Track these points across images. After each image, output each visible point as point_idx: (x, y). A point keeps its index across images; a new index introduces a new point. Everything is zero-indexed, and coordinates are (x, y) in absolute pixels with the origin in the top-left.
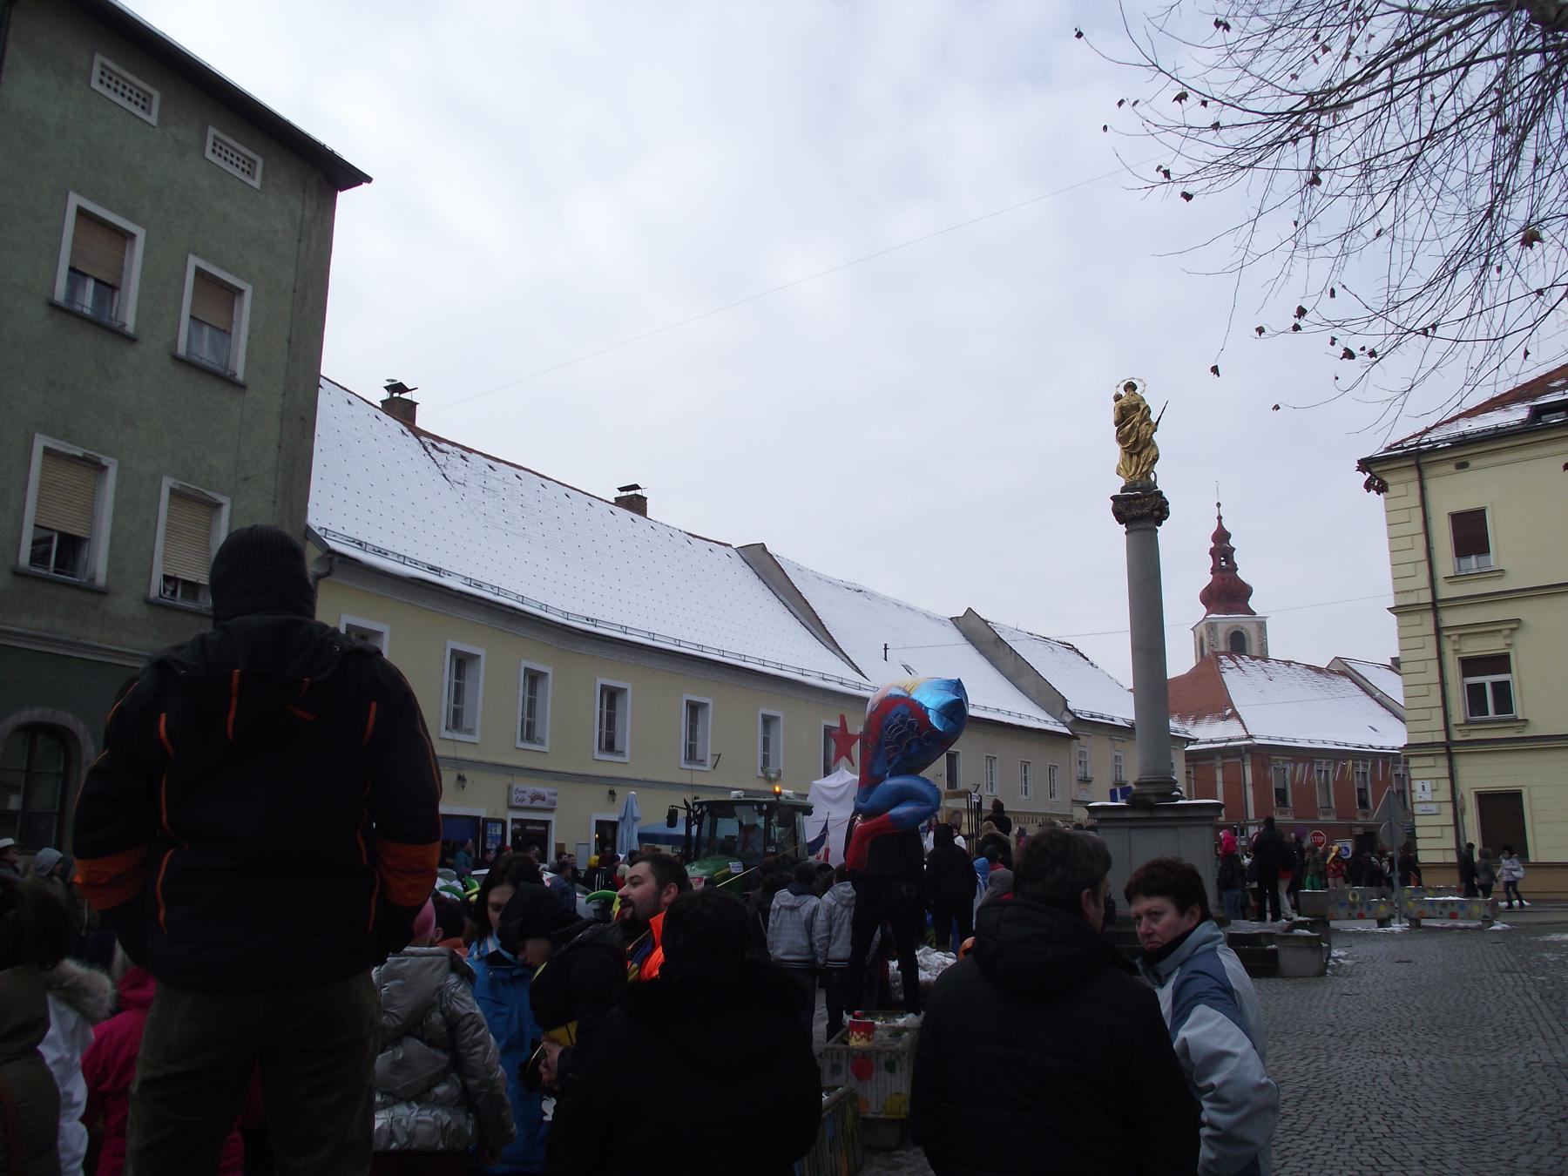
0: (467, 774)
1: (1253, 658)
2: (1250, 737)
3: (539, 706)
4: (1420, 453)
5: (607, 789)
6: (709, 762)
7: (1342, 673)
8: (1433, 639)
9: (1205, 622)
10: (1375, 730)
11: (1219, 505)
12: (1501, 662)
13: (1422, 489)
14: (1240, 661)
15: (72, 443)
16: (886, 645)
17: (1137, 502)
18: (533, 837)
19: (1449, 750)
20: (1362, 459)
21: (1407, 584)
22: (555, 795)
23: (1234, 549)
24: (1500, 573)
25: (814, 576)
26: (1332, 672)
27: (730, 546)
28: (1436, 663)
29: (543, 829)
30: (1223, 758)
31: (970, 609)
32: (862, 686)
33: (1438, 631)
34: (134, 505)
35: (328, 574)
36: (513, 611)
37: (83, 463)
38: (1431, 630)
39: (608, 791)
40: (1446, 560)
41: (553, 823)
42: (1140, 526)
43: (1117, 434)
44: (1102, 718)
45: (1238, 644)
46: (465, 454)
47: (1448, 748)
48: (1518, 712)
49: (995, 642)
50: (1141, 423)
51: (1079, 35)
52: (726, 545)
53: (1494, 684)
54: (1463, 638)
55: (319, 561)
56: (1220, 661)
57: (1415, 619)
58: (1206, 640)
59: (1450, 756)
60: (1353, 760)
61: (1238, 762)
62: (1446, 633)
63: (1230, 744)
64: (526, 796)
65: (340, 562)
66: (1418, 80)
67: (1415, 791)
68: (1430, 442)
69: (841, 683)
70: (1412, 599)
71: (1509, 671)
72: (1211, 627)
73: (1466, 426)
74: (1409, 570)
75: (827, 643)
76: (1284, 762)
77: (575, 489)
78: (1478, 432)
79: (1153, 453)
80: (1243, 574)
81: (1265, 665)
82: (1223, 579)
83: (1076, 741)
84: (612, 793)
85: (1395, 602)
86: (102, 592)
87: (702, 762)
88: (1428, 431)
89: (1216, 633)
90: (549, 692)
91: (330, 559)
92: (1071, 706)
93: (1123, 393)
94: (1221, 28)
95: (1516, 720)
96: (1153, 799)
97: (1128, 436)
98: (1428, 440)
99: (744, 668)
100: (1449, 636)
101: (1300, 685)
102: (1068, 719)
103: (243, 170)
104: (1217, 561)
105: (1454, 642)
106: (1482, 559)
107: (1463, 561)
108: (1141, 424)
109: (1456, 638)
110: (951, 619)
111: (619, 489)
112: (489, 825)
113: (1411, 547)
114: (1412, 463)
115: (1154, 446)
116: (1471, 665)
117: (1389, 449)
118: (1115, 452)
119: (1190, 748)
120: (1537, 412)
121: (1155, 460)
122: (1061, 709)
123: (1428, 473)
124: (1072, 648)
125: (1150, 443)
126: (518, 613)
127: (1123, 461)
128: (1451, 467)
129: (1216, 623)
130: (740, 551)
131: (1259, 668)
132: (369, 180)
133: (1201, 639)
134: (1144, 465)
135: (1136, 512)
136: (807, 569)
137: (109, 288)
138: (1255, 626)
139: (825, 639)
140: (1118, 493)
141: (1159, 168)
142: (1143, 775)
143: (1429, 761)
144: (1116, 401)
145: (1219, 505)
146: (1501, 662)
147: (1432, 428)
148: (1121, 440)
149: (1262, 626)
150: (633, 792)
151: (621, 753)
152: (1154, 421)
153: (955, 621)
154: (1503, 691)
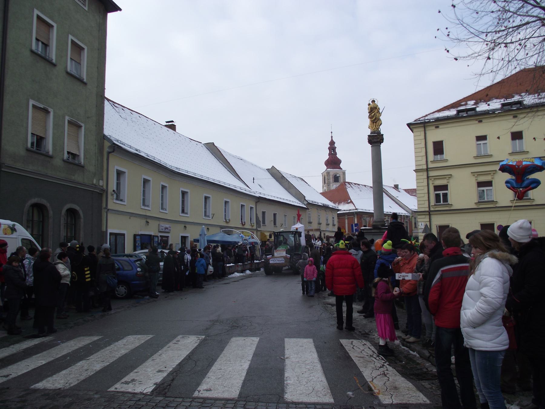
0: (149, 221)
2: (356, 209)
3: (164, 197)
4: (425, 123)
5: (184, 225)
6: (211, 216)
8: (426, 180)
9: (326, 171)
10: (391, 207)
11: (332, 132)
12: (445, 187)
15: (40, 103)
16: (254, 178)
17: (376, 137)
18: (164, 242)
19: (429, 213)
20: (408, 124)
21: (419, 163)
22: (170, 227)
23: (336, 148)
24: (446, 161)
27: (201, 143)
29: (167, 239)
30: (348, 216)
31: (273, 166)
33: (428, 177)
34: (58, 126)
35: (113, 152)
36: (160, 165)
37: (42, 110)
38: (426, 177)
39: (184, 226)
41: (170, 237)
42: (376, 145)
44: (315, 202)
46: (123, 108)
47: (429, 213)
48: (450, 202)
49: (282, 178)
51: (439, 12)
53: (443, 193)
54: (435, 180)
55: (110, 147)
56: (346, 185)
57: (421, 174)
58: (326, 177)
59: (430, 215)
60: (388, 217)
61: (353, 217)
62: (430, 178)
63: (350, 211)
64: (163, 228)
65: (117, 147)
67: (419, 225)
68: (428, 119)
70: (420, 168)
72: (328, 173)
74: (420, 158)
75: (236, 177)
76: (367, 217)
77: (156, 122)
78: (442, 117)
79: (381, 123)
80: (339, 156)
81: (359, 186)
82: (332, 157)
83: (308, 210)
84: (185, 227)
86: (51, 157)
87: (208, 216)
88: (426, 116)
89: (330, 175)
90: (168, 191)
91: (114, 147)
92: (306, 199)
95: (449, 204)
96: (380, 226)
97: (373, 117)
99: (219, 185)
100: (431, 179)
101: (369, 193)
102: (306, 203)
103: (82, 3)
104: (331, 151)
105: (432, 181)
106: (441, 156)
107: (436, 156)
108: (377, 113)
109: (433, 180)
110: (267, 169)
111: (166, 122)
112: (155, 237)
114: (423, 125)
115: (381, 120)
116: (437, 188)
117: (416, 121)
118: (368, 122)
119: (338, 212)
120: (459, 112)
121: (381, 125)
122: (303, 200)
123: (427, 129)
124: (303, 180)
125: (379, 120)
126: (162, 166)
128: (434, 128)
129: (330, 172)
132: (120, 10)
133: (325, 177)
134: (378, 126)
135: (375, 140)
137: (46, 46)
138: (342, 173)
139: (236, 175)
140: (370, 134)
141: (446, 50)
142: (377, 219)
143: (423, 216)
145: (332, 132)
146: (445, 187)
147: (428, 115)
148: (370, 117)
149: (344, 173)
150: (204, 226)
151: (187, 213)
152: (381, 112)
154: (445, 195)
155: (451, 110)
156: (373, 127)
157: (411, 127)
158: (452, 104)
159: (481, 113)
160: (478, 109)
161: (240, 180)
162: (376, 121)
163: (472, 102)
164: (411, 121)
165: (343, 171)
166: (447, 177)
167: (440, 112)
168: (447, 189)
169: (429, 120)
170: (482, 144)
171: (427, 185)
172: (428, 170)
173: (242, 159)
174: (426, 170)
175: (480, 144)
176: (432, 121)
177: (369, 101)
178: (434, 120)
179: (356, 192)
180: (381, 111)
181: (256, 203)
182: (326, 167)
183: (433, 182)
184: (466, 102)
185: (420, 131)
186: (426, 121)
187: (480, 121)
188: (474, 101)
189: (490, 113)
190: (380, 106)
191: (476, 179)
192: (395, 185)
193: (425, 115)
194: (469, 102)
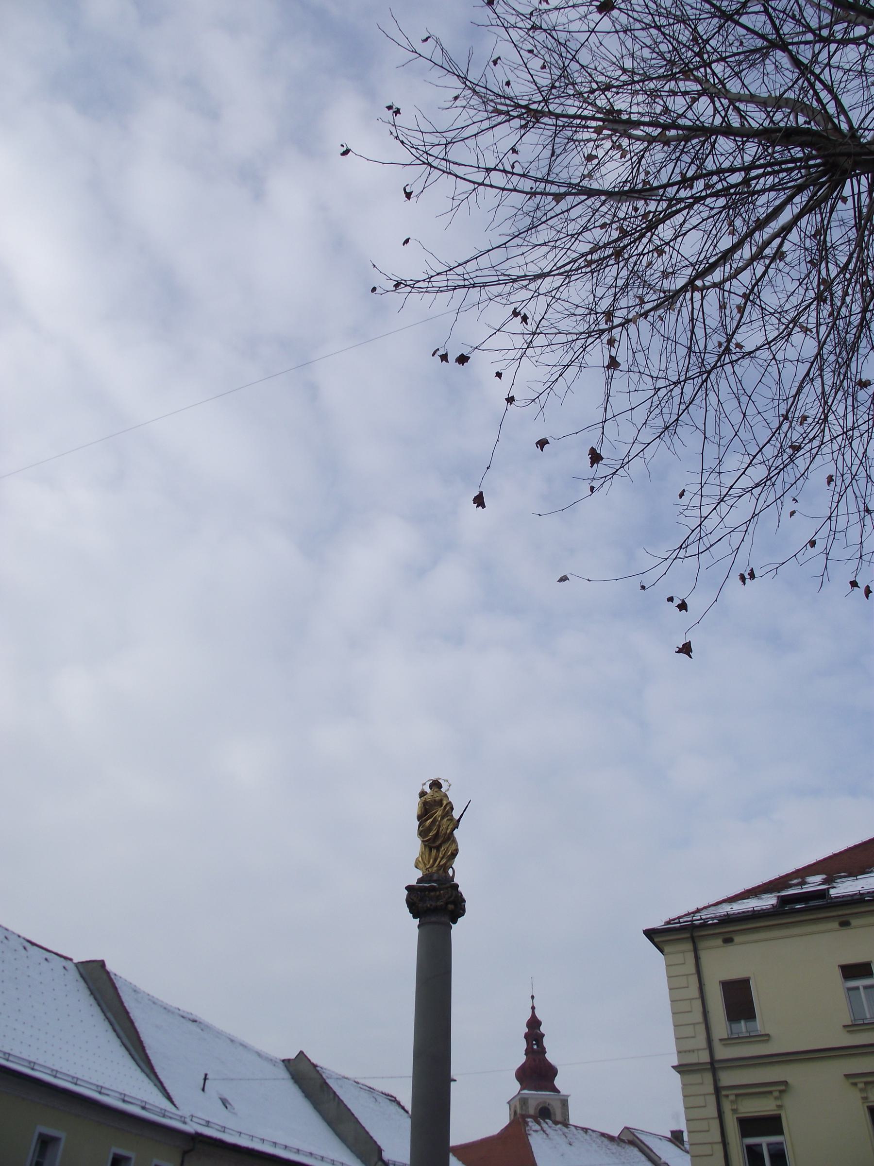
1: (556, 1123)
7: (632, 1143)
9: (519, 1097)
11: (533, 997)
13: (697, 959)
14: (544, 1125)
16: (206, 1075)
17: (432, 894)
24: (766, 1038)
25: (149, 1000)
26: (623, 1141)
27: (71, 960)
28: (717, 1122)
31: (301, 1053)
32: (166, 1114)
38: (711, 1089)
40: (720, 1026)
42: (433, 919)
43: (419, 827)
45: (544, 1113)
50: (443, 818)
52: (66, 958)
53: (768, 1145)
56: (527, 1123)
57: (695, 1078)
62: (724, 1093)
66: (743, 173)
68: (701, 919)
69: (144, 1108)
70: (692, 1059)
71: (780, 1132)
72: (524, 1101)
73: (726, 909)
79: (453, 847)
81: (565, 1130)
85: (678, 1060)
88: (698, 911)
89: (528, 1108)
93: (428, 790)
94: (519, 318)
97: (429, 829)
98: (699, 918)
100: (727, 1096)
106: (750, 1024)
107: (735, 1026)
110: (283, 1061)
113: (689, 1009)
114: (688, 935)
117: (668, 923)
118: (415, 846)
121: (454, 854)
123: (701, 945)
125: (450, 838)
127: (422, 854)
128: (719, 942)
130: (80, 967)
131: (561, 1133)
134: (442, 858)
136: (144, 992)
140: (414, 882)
144: (420, 798)
145: (533, 997)
147: (702, 909)
148: (422, 833)
149: (564, 1103)
153: (287, 1062)
155: (764, 896)
156: (429, 862)
157: (656, 940)
158: (765, 884)
159: (843, 901)
160: (833, 892)
161: (153, 1077)
162: (438, 843)
163: (819, 878)
164: (657, 923)
165: (562, 1098)
166: (776, 1091)
167: (735, 902)
168: (780, 1132)
169: (702, 921)
170: (861, 988)
171: (716, 1114)
172: (717, 1065)
173: (195, 1021)
174: (709, 1067)
175: (857, 988)
176: (710, 922)
177: (425, 784)
178: (715, 921)
179: (555, 1147)
180: (456, 815)
181: (185, 1153)
182: (518, 1086)
183: (735, 1107)
184: (803, 878)
185: (683, 952)
186: (694, 922)
187: (845, 924)
188: (824, 876)
189: (866, 899)
190: (457, 799)
191: (865, 1099)
192: (673, 1132)
193: (693, 909)
194: (810, 879)
